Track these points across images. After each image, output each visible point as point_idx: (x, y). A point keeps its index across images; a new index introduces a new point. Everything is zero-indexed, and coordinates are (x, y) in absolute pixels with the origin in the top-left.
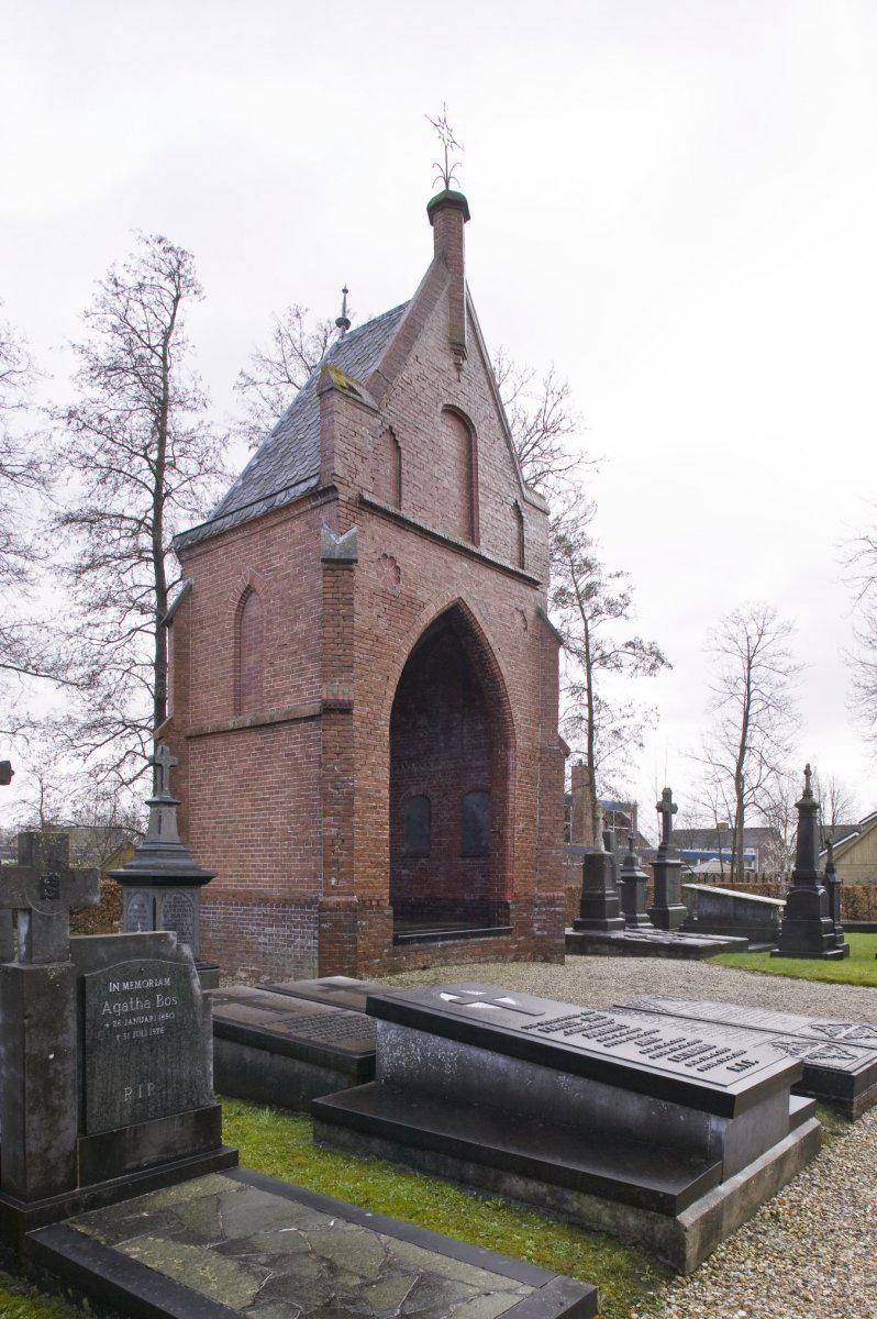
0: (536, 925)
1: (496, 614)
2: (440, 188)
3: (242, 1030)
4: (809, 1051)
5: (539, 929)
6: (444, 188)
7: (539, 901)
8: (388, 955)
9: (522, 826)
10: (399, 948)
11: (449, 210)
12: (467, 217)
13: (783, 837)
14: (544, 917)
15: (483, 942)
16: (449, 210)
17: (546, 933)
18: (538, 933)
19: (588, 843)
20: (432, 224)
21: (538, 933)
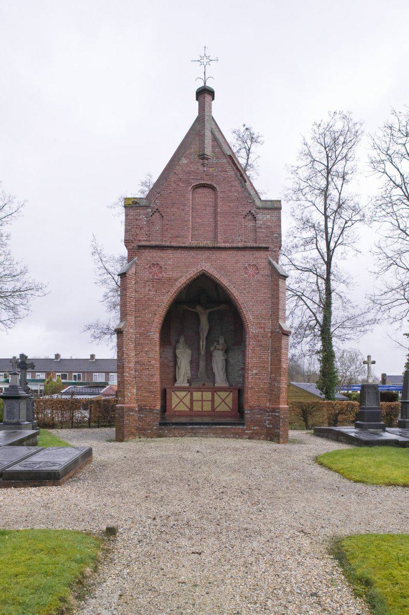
0: (267, 422)
1: (234, 276)
2: (202, 85)
3: (41, 473)
4: (38, 466)
5: (269, 424)
6: (204, 85)
7: (268, 410)
8: (156, 429)
9: (255, 372)
10: (163, 427)
11: (205, 94)
12: (213, 99)
13: (387, 429)
14: (271, 418)
15: (222, 428)
16: (205, 94)
17: (271, 426)
18: (268, 426)
19: (263, 504)
20: (197, 100)
21: (268, 426)
